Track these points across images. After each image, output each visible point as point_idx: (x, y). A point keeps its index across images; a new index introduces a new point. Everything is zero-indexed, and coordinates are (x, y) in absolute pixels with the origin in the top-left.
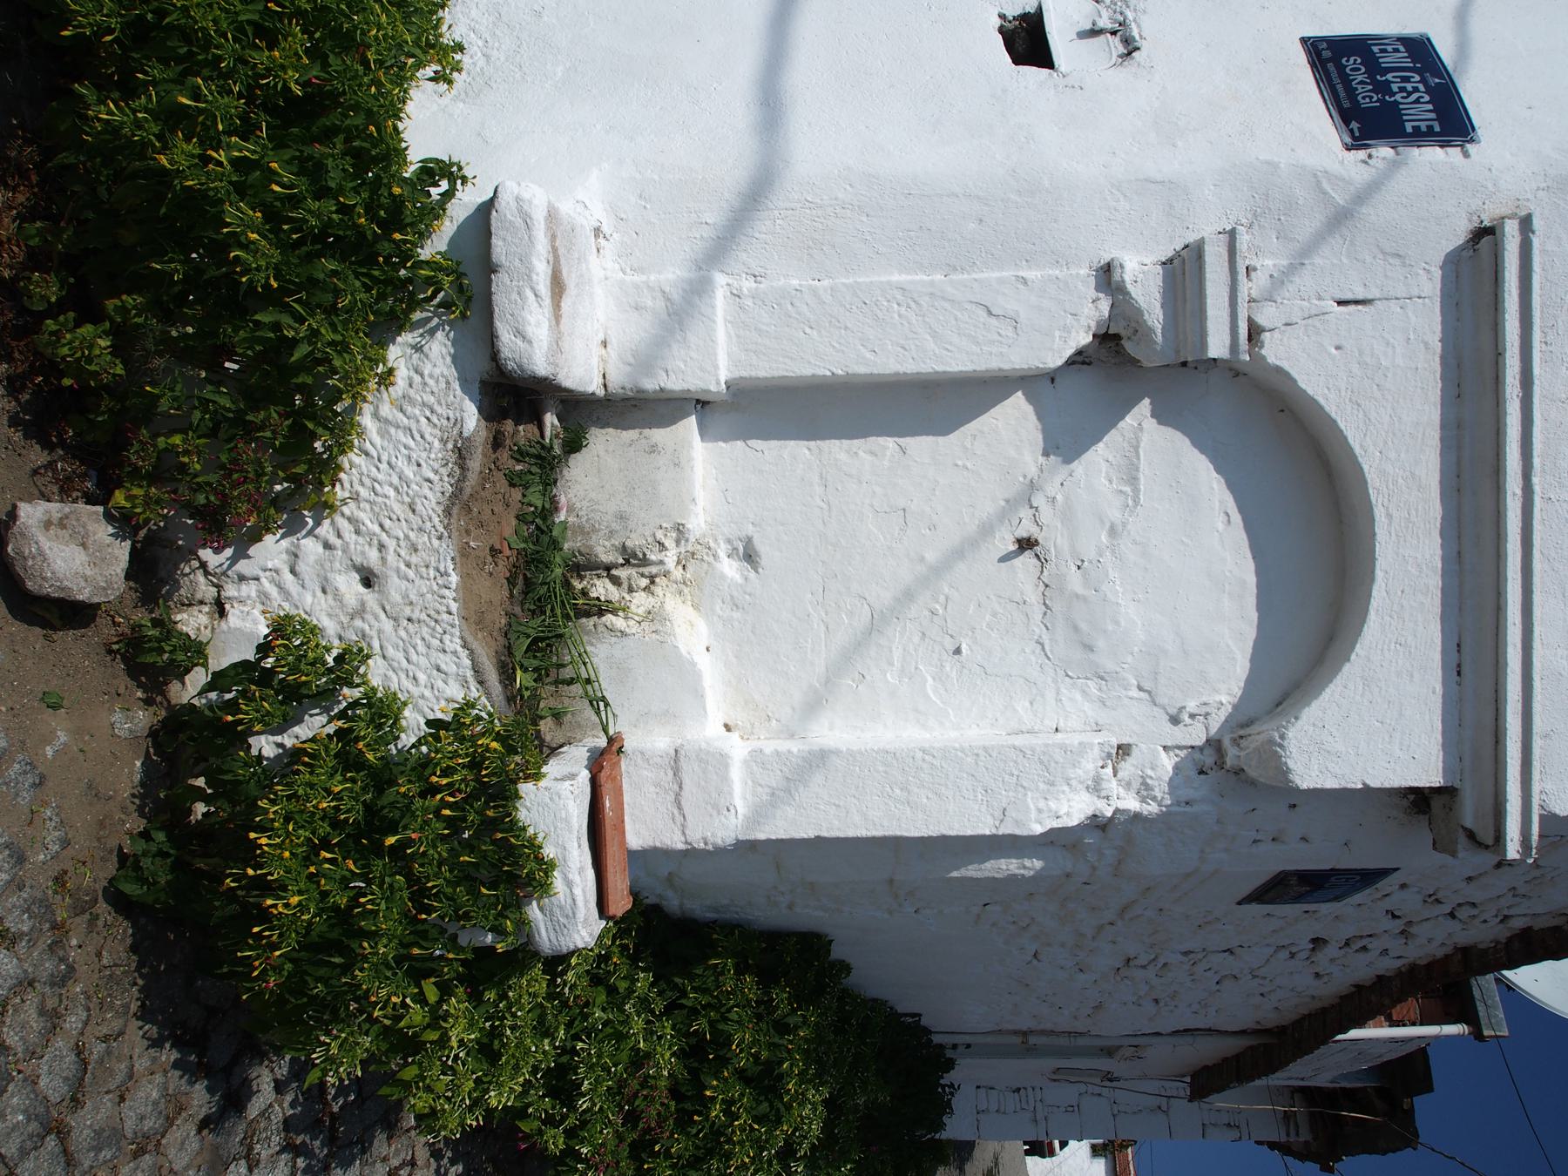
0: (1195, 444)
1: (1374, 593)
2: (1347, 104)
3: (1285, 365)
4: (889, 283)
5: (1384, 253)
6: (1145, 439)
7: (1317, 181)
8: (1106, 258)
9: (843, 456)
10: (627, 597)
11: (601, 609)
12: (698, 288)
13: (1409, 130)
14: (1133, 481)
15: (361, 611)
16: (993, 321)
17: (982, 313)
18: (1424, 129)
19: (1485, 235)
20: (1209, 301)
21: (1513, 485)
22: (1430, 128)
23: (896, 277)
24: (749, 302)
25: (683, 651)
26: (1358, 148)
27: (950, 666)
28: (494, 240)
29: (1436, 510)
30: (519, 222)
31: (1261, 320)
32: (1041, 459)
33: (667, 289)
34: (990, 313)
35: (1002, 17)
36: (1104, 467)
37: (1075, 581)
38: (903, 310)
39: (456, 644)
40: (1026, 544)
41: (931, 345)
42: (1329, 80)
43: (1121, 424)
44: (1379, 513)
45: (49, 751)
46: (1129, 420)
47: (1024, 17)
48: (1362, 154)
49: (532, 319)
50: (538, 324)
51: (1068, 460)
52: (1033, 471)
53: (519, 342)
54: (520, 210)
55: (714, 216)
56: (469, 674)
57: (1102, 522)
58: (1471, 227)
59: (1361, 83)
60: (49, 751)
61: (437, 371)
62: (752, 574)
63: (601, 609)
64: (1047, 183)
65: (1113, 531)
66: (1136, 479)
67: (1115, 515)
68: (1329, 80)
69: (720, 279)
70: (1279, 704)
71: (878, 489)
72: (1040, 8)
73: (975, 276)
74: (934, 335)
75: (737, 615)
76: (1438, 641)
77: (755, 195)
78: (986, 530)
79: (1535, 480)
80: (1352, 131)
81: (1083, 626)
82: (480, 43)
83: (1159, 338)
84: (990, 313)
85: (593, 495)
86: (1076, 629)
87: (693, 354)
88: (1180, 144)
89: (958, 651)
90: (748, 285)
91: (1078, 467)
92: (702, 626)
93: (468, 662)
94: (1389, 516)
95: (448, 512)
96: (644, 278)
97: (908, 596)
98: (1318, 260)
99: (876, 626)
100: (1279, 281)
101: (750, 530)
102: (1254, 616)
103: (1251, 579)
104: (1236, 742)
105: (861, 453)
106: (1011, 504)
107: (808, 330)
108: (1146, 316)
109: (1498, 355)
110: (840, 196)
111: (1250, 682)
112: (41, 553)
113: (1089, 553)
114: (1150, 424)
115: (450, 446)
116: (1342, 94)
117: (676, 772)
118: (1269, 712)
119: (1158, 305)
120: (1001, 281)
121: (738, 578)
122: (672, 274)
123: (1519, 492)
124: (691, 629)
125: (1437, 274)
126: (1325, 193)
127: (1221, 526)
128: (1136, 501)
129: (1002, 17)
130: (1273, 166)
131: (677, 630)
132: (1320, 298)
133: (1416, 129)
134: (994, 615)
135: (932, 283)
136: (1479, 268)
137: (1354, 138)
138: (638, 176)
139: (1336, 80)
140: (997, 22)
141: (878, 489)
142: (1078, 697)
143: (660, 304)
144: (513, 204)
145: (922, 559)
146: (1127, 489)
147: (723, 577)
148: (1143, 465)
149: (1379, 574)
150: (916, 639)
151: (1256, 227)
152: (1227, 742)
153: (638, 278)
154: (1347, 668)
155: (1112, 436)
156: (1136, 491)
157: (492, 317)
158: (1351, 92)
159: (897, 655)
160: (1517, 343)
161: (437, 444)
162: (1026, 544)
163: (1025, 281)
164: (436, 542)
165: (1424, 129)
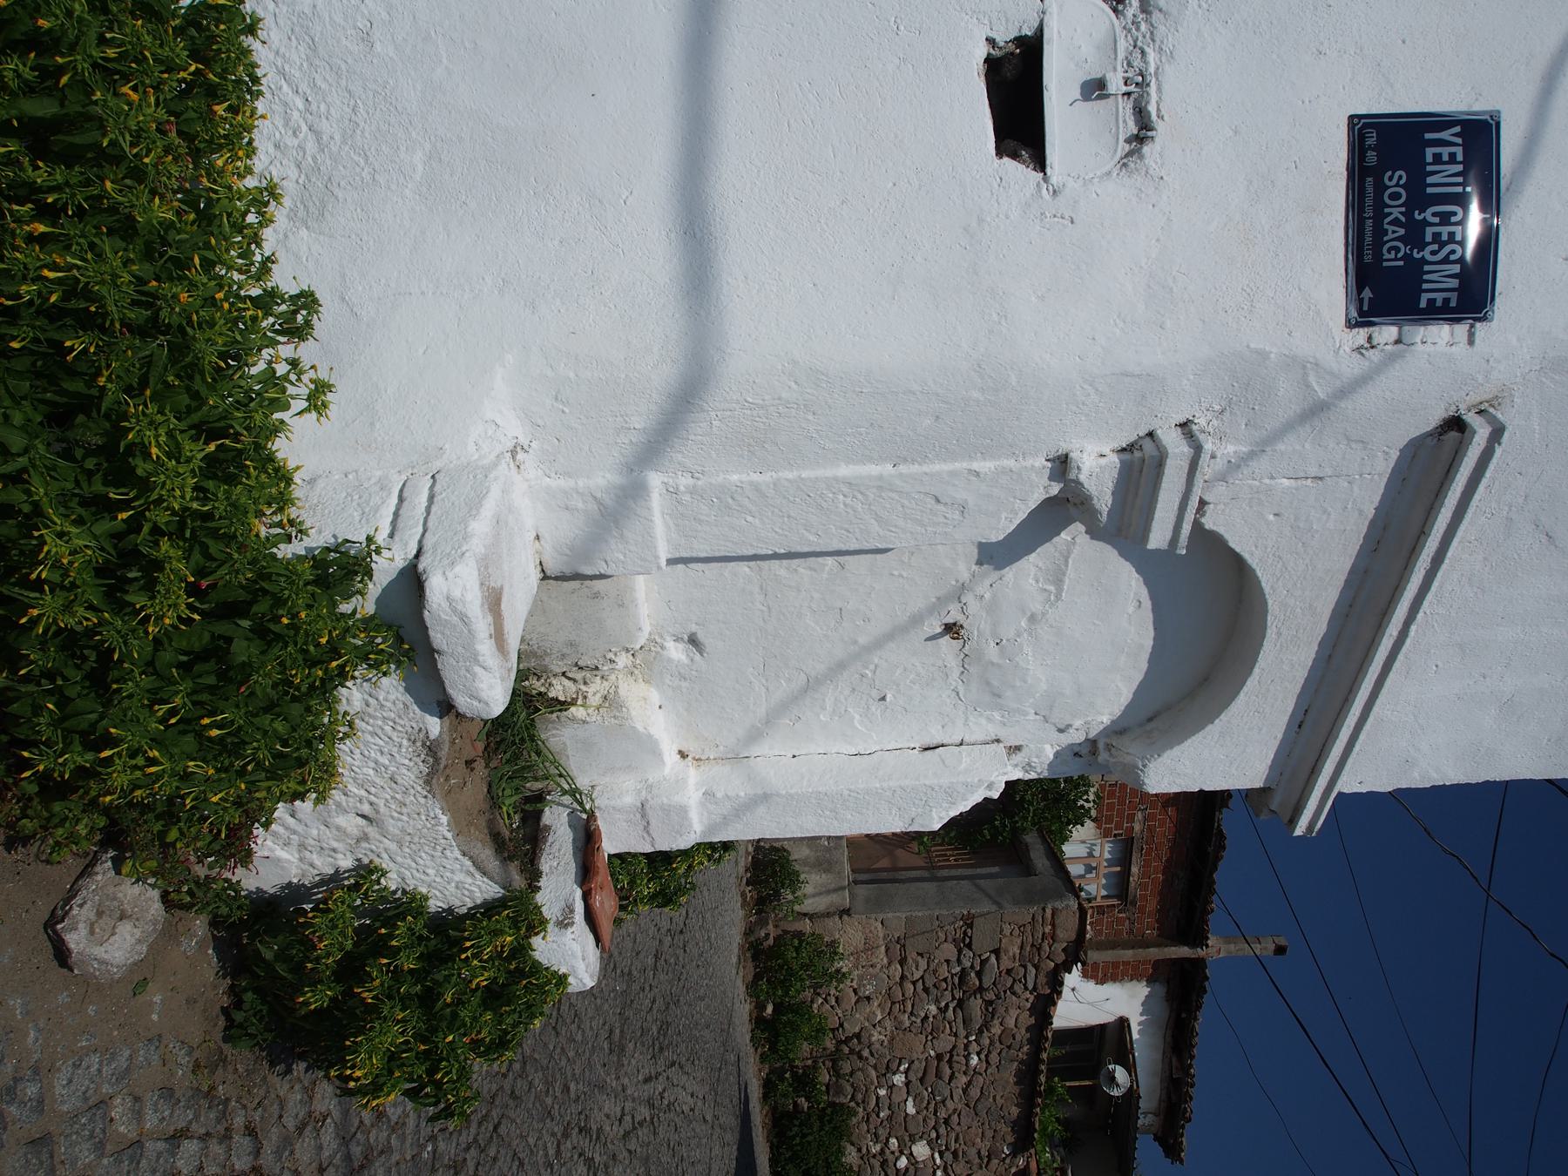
0: (1121, 554)
1: (1248, 683)
2: (1368, 259)
3: (1221, 530)
4: (836, 479)
5: (1348, 439)
6: (1076, 551)
7: (1300, 366)
8: (1064, 447)
9: (783, 572)
10: (584, 688)
11: (562, 705)
12: (631, 493)
13: (1423, 304)
14: (1058, 582)
15: (365, 837)
16: (941, 507)
17: (930, 501)
18: (1439, 303)
19: (1456, 424)
20: (1159, 506)
21: (1393, 630)
22: (1446, 301)
23: (844, 471)
24: (687, 498)
25: (640, 727)
26: (1359, 325)
27: (875, 708)
28: (431, 633)
29: (1322, 628)
30: (455, 619)
31: (1206, 498)
32: (974, 567)
33: (599, 495)
34: (938, 501)
35: (991, 41)
36: (1033, 570)
37: (992, 652)
38: (848, 501)
39: (457, 853)
40: (952, 629)
41: (875, 527)
42: (1361, 210)
43: (1056, 539)
44: (1271, 633)
45: (155, 1017)
46: (1065, 536)
47: (1020, 41)
48: (1361, 335)
49: (483, 686)
50: (491, 687)
51: (999, 567)
52: (965, 576)
53: (475, 703)
54: (455, 610)
55: (641, 417)
56: (472, 869)
57: (1024, 612)
58: (1445, 415)
59: (1395, 222)
60: (155, 1017)
61: (392, 697)
62: (697, 657)
63: (562, 705)
64: (1013, 380)
65: (1032, 619)
66: (1061, 581)
67: (1036, 607)
68: (1361, 210)
69: (655, 480)
70: (1150, 720)
71: (816, 595)
72: (1040, 31)
73: (925, 468)
74: (878, 519)
75: (684, 684)
76: (1290, 710)
77: (687, 397)
78: (917, 620)
79: (1413, 628)
80: (1361, 301)
81: (995, 683)
82: (300, 104)
83: (1104, 518)
84: (938, 501)
85: (542, 630)
86: (988, 683)
87: (633, 548)
88: (1168, 324)
89: (883, 699)
90: (684, 481)
91: (1009, 573)
92: (655, 696)
93: (469, 863)
94: (1279, 634)
95: (428, 782)
96: (571, 483)
97: (841, 666)
98: (1281, 447)
99: (811, 686)
100: (1234, 466)
101: (694, 628)
102: (1145, 666)
103: (1148, 643)
104: (1109, 747)
105: (801, 570)
106: (942, 601)
107: (749, 519)
108: (1095, 501)
109: (1423, 533)
110: (784, 395)
111: (1130, 707)
112: (102, 962)
113: (1007, 632)
114: (1083, 539)
115: (419, 744)
116: (1368, 239)
117: (643, 816)
118: (1141, 725)
119: (1109, 492)
120: (953, 474)
121: (683, 658)
122: (603, 478)
123: (1395, 634)
124: (650, 710)
125: (1395, 455)
126: (1308, 386)
127: (1131, 610)
128: (1058, 597)
129: (991, 41)
130: (1263, 355)
131: (634, 713)
132: (1272, 478)
133: (1431, 302)
134: (918, 675)
135: (880, 477)
136: (1438, 461)
137: (1361, 313)
138: (549, 373)
139: (1369, 213)
140: (982, 51)
141: (816, 595)
142: (984, 721)
143: (592, 506)
144: (445, 605)
145: (856, 642)
146: (1052, 588)
147: (670, 660)
148: (1070, 571)
149: (1256, 670)
150: (847, 692)
151: (1227, 414)
152: (1101, 745)
153: (562, 483)
154: (1210, 727)
155: (1047, 548)
156: (1059, 591)
157: (442, 683)
158: (1378, 243)
159: (829, 704)
160: (1439, 536)
161: (405, 742)
162: (952, 629)
163: (977, 474)
164: (423, 801)
165: (1439, 303)
